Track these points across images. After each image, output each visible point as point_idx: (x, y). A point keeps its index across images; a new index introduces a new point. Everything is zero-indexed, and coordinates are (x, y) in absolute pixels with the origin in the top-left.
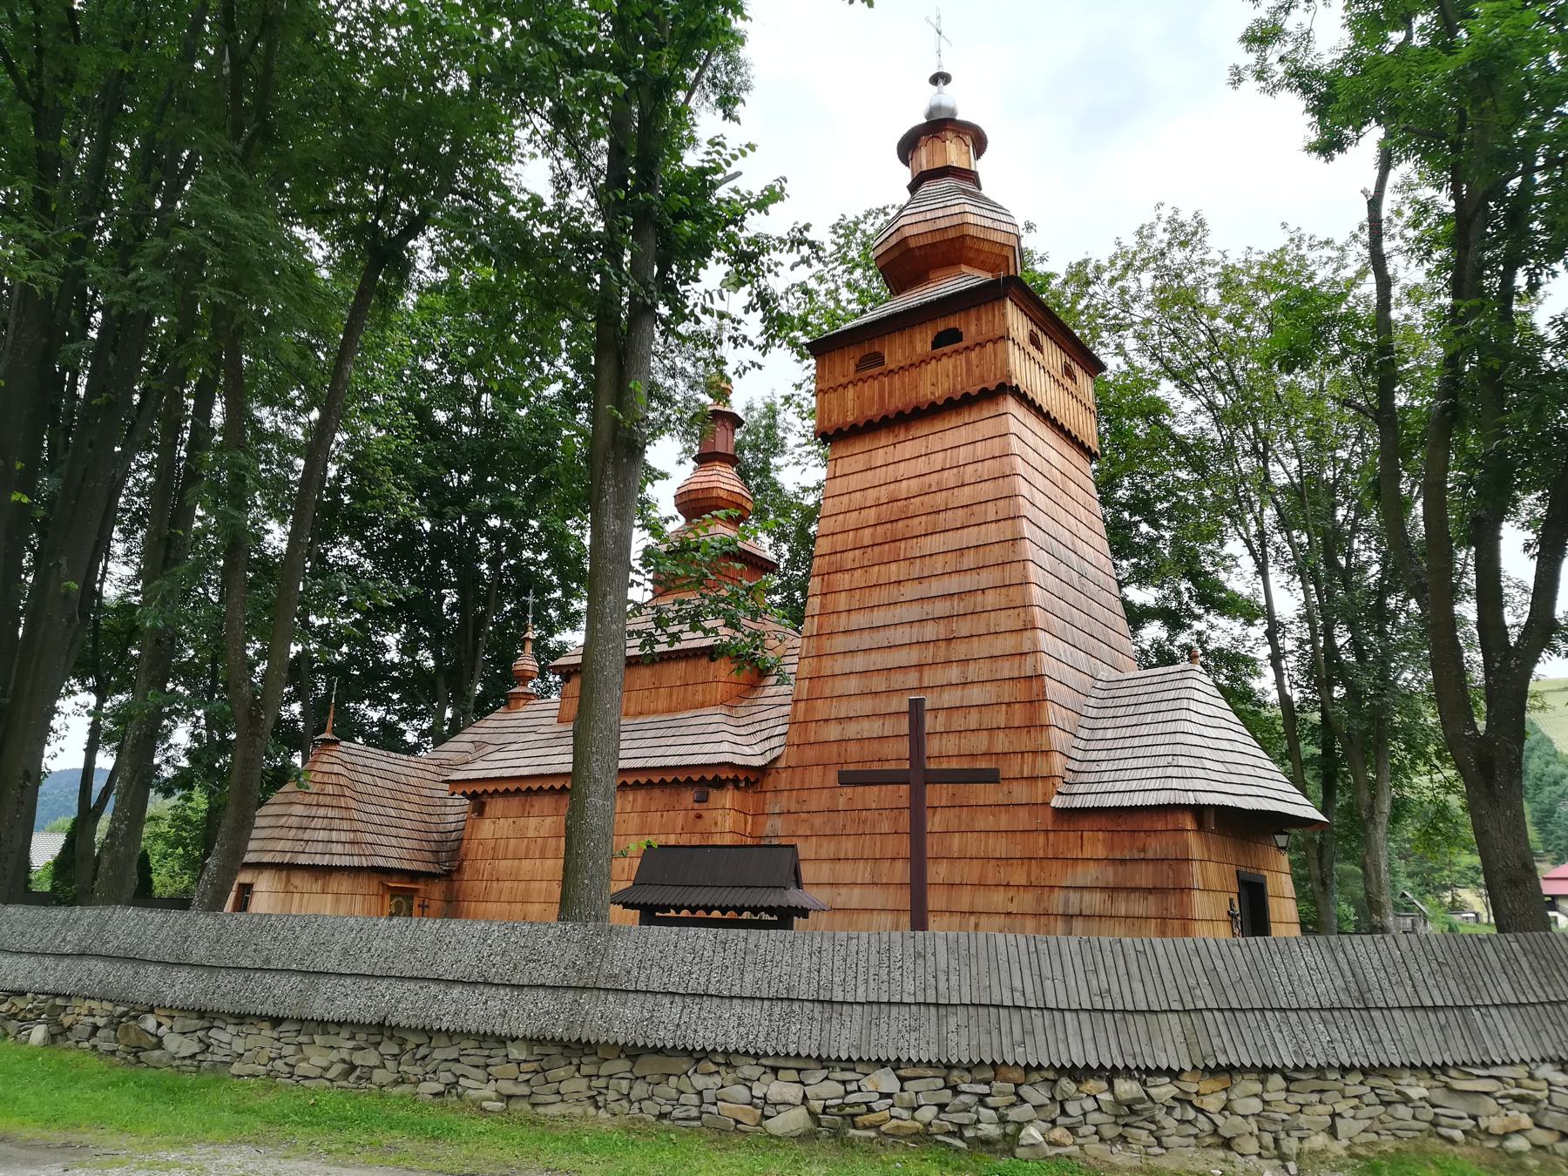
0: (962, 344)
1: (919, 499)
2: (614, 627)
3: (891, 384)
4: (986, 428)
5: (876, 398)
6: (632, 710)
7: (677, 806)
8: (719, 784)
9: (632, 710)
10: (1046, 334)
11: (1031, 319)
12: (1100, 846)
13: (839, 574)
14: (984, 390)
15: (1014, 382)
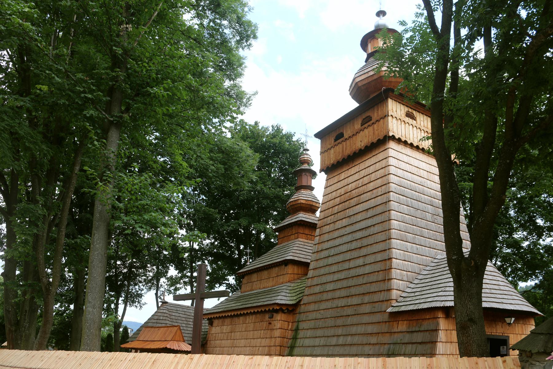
0: (371, 122)
1: (355, 191)
2: (98, 246)
3: (346, 144)
4: (381, 156)
5: (341, 152)
6: (261, 287)
7: (264, 320)
8: (277, 311)
10: (416, 110)
11: (407, 106)
13: (326, 226)
14: (379, 140)
15: (391, 134)
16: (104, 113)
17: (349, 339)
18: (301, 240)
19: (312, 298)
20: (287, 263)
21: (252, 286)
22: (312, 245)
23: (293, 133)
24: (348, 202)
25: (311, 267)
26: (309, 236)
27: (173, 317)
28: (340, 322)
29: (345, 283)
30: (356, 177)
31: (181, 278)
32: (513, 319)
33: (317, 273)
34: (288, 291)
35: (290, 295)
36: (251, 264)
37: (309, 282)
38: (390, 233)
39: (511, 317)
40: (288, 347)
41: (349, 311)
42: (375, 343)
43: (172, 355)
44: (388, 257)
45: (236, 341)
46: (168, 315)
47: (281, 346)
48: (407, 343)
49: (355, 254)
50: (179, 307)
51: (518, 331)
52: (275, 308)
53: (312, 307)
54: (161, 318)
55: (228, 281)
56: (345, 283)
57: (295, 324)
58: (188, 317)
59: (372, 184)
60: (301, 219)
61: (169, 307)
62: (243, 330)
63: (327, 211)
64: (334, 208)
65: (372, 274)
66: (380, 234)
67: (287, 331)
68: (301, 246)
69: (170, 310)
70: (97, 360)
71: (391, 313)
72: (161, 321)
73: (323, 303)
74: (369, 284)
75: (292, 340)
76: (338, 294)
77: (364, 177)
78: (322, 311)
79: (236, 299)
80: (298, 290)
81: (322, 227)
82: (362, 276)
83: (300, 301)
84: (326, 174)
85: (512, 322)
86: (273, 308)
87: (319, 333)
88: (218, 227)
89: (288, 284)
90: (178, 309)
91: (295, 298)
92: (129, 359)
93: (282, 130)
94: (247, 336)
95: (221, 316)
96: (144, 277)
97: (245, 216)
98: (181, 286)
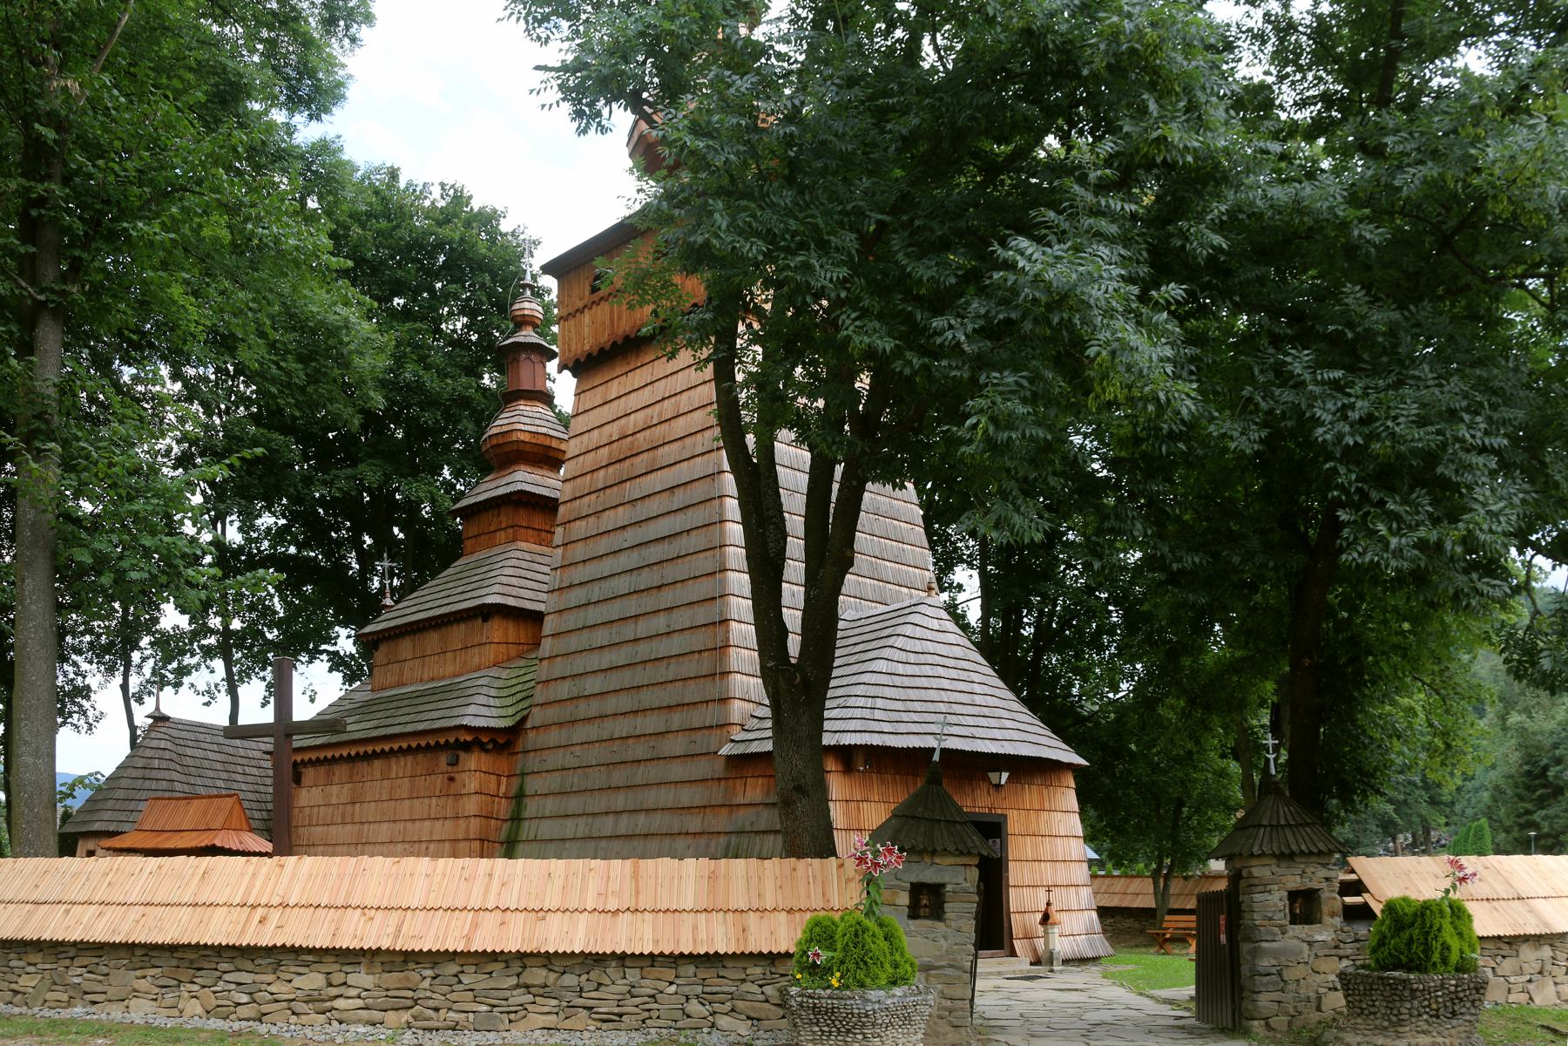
1: (642, 434)
2: (34, 607)
5: (607, 323)
6: (425, 677)
8: (467, 747)
9: (425, 677)
12: (758, 790)
13: (578, 522)
16: (24, 284)
17: (642, 819)
18: (522, 545)
19: (552, 714)
20: (486, 612)
21: (401, 673)
22: (547, 569)
23: (500, 208)
24: (627, 462)
25: (549, 625)
26: (544, 535)
27: (189, 761)
28: (619, 776)
29: (626, 678)
30: (645, 396)
31: (195, 635)
32: (1005, 776)
33: (562, 645)
34: (493, 692)
35: (497, 702)
36: (395, 614)
37: (544, 671)
38: (723, 556)
39: (1000, 770)
40: (502, 843)
41: (639, 750)
42: (698, 830)
43: (241, 860)
44: (721, 615)
45: (366, 826)
46: (174, 756)
47: (482, 840)
48: (764, 832)
49: (647, 602)
50: (202, 730)
51: (1031, 802)
52: (462, 739)
53: (554, 737)
54: (156, 763)
55: (335, 644)
56: (626, 678)
57: (516, 781)
58: (231, 759)
59: (681, 420)
60: (519, 487)
61: (175, 733)
62: (384, 797)
63: (579, 481)
64: (595, 474)
65: (687, 658)
66: (702, 555)
67: (497, 799)
68: (524, 564)
69: (177, 741)
70: (76, 875)
71: (731, 759)
72: (154, 774)
73: (579, 726)
74: (681, 683)
75: (509, 823)
76: (612, 704)
77: (663, 399)
78: (578, 748)
79: (360, 711)
80: (519, 688)
81: (569, 522)
82: (665, 661)
83: (524, 719)
84: (574, 376)
85: (1003, 782)
86: (457, 740)
87: (574, 804)
88: (296, 486)
89: (494, 672)
90: (201, 737)
91: (511, 711)
92: (148, 871)
93: (470, 197)
94: (395, 813)
95: (322, 757)
96: (88, 638)
97: (371, 456)
98: (194, 661)
